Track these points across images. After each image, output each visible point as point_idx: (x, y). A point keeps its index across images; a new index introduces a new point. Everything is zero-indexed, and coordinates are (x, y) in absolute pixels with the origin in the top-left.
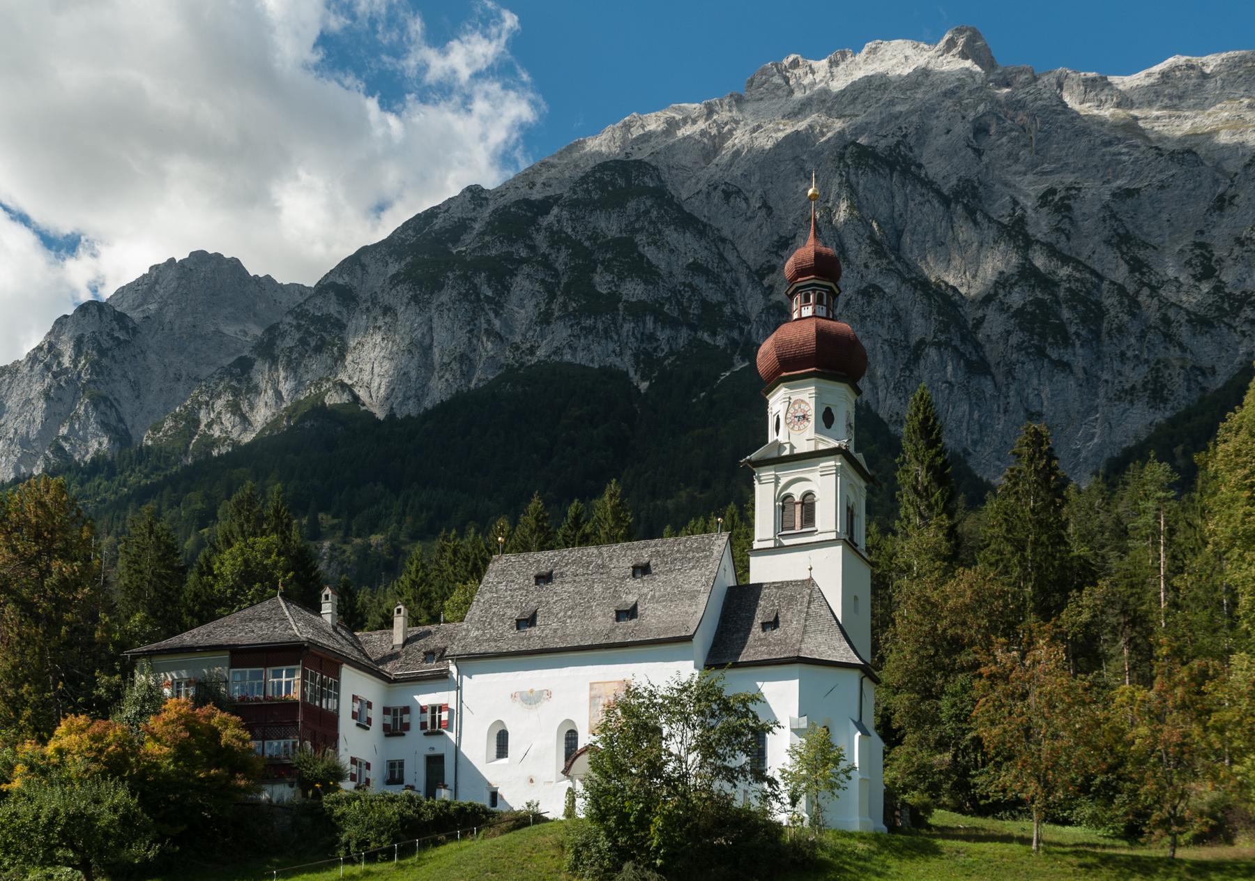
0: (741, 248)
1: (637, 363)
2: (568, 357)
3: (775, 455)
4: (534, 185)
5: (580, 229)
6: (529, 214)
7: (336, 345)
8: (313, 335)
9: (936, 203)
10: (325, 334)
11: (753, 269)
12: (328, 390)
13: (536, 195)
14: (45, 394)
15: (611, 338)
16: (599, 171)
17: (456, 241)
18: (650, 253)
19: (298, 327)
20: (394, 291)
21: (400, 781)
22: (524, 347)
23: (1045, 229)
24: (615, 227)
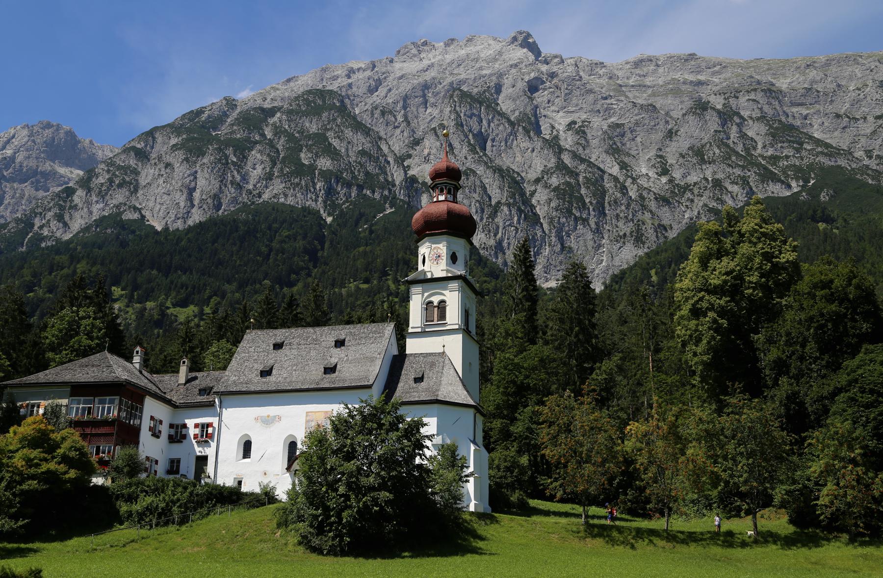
0: (391, 143)
1: (326, 207)
2: (282, 200)
3: (422, 277)
5: (293, 126)
6: (262, 116)
7: (132, 184)
10: (126, 177)
11: (398, 155)
12: (125, 211)
13: (267, 105)
15: (310, 191)
17: (215, 129)
18: (335, 143)
19: (108, 171)
20: (173, 154)
21: (177, 472)
22: (255, 193)
23: (571, 143)
24: (315, 127)
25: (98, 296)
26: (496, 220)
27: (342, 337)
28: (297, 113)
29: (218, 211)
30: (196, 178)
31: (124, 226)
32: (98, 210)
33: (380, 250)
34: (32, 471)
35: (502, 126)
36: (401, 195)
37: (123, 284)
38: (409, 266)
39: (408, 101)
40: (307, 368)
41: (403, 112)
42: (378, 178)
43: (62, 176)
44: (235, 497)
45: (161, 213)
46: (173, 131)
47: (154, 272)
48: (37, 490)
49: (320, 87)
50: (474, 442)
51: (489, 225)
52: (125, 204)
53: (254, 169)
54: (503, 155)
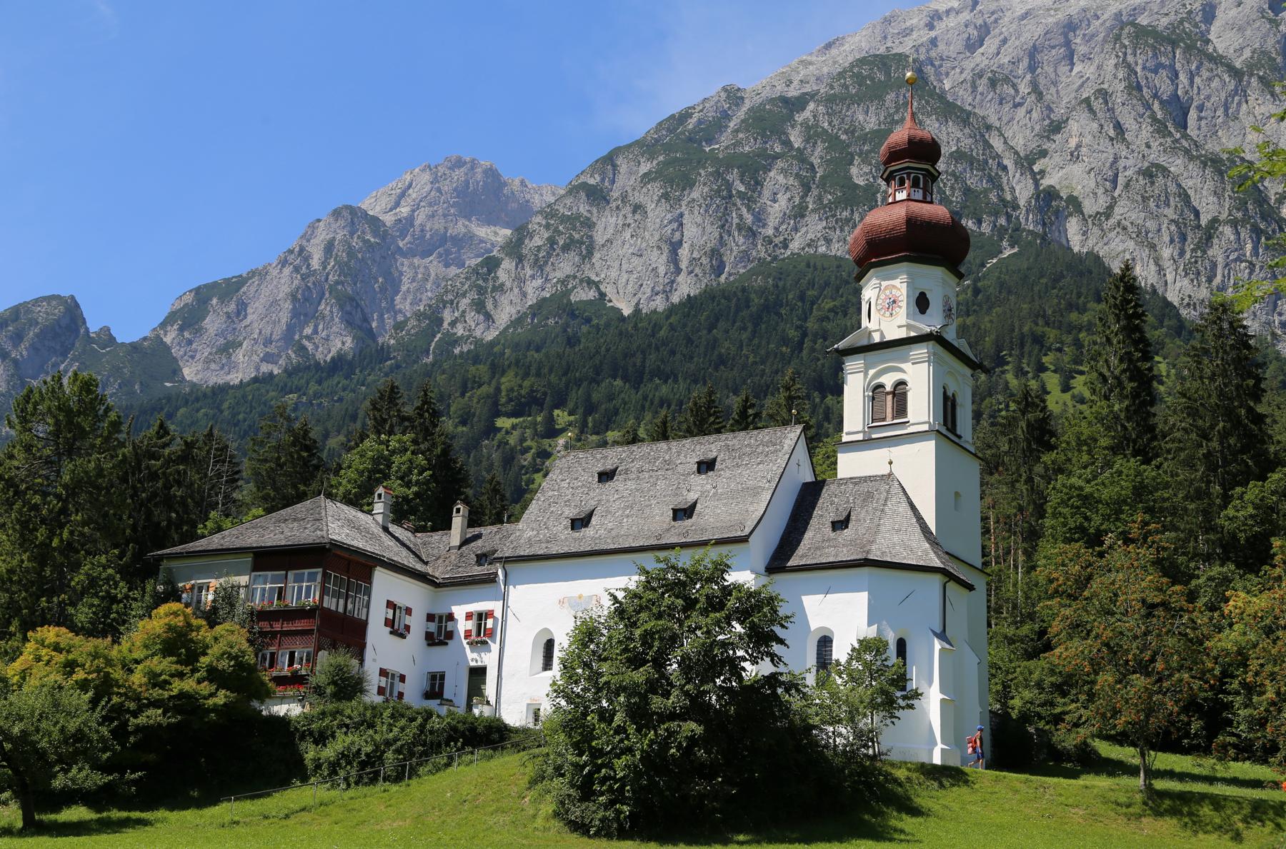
0: (1008, 134)
2: (822, 249)
3: (865, 342)
4: (791, 83)
5: (836, 122)
6: (784, 111)
7: (584, 243)
8: (562, 233)
9: (1226, 78)
12: (575, 287)
13: (793, 92)
14: (292, 295)
16: (857, 66)
19: (547, 227)
20: (645, 190)
22: (777, 241)
24: (873, 120)
25: (421, 416)
26: (1210, 253)
27: (711, 456)
28: (843, 100)
29: (719, 276)
30: (681, 225)
31: (572, 312)
32: (535, 290)
33: (991, 321)
34: (156, 693)
35: (1217, 79)
36: (1030, 223)
37: (571, 405)
38: (1042, 346)
39: (1039, 57)
40: (647, 511)
41: (1028, 77)
42: (986, 196)
43: (482, 241)
44: (496, 736)
45: (629, 287)
46: (644, 152)
47: (618, 382)
48: (160, 725)
49: (882, 50)
50: (942, 636)
51: (1196, 262)
52: (575, 277)
53: (775, 201)
54: (1220, 133)
